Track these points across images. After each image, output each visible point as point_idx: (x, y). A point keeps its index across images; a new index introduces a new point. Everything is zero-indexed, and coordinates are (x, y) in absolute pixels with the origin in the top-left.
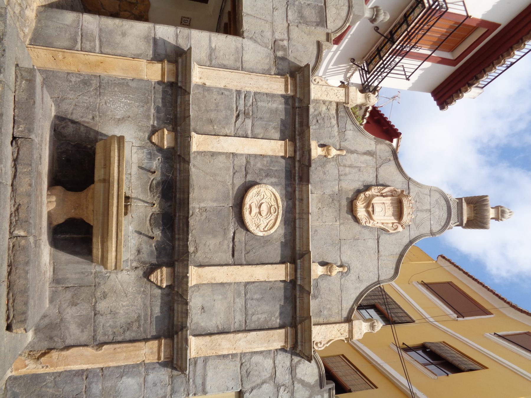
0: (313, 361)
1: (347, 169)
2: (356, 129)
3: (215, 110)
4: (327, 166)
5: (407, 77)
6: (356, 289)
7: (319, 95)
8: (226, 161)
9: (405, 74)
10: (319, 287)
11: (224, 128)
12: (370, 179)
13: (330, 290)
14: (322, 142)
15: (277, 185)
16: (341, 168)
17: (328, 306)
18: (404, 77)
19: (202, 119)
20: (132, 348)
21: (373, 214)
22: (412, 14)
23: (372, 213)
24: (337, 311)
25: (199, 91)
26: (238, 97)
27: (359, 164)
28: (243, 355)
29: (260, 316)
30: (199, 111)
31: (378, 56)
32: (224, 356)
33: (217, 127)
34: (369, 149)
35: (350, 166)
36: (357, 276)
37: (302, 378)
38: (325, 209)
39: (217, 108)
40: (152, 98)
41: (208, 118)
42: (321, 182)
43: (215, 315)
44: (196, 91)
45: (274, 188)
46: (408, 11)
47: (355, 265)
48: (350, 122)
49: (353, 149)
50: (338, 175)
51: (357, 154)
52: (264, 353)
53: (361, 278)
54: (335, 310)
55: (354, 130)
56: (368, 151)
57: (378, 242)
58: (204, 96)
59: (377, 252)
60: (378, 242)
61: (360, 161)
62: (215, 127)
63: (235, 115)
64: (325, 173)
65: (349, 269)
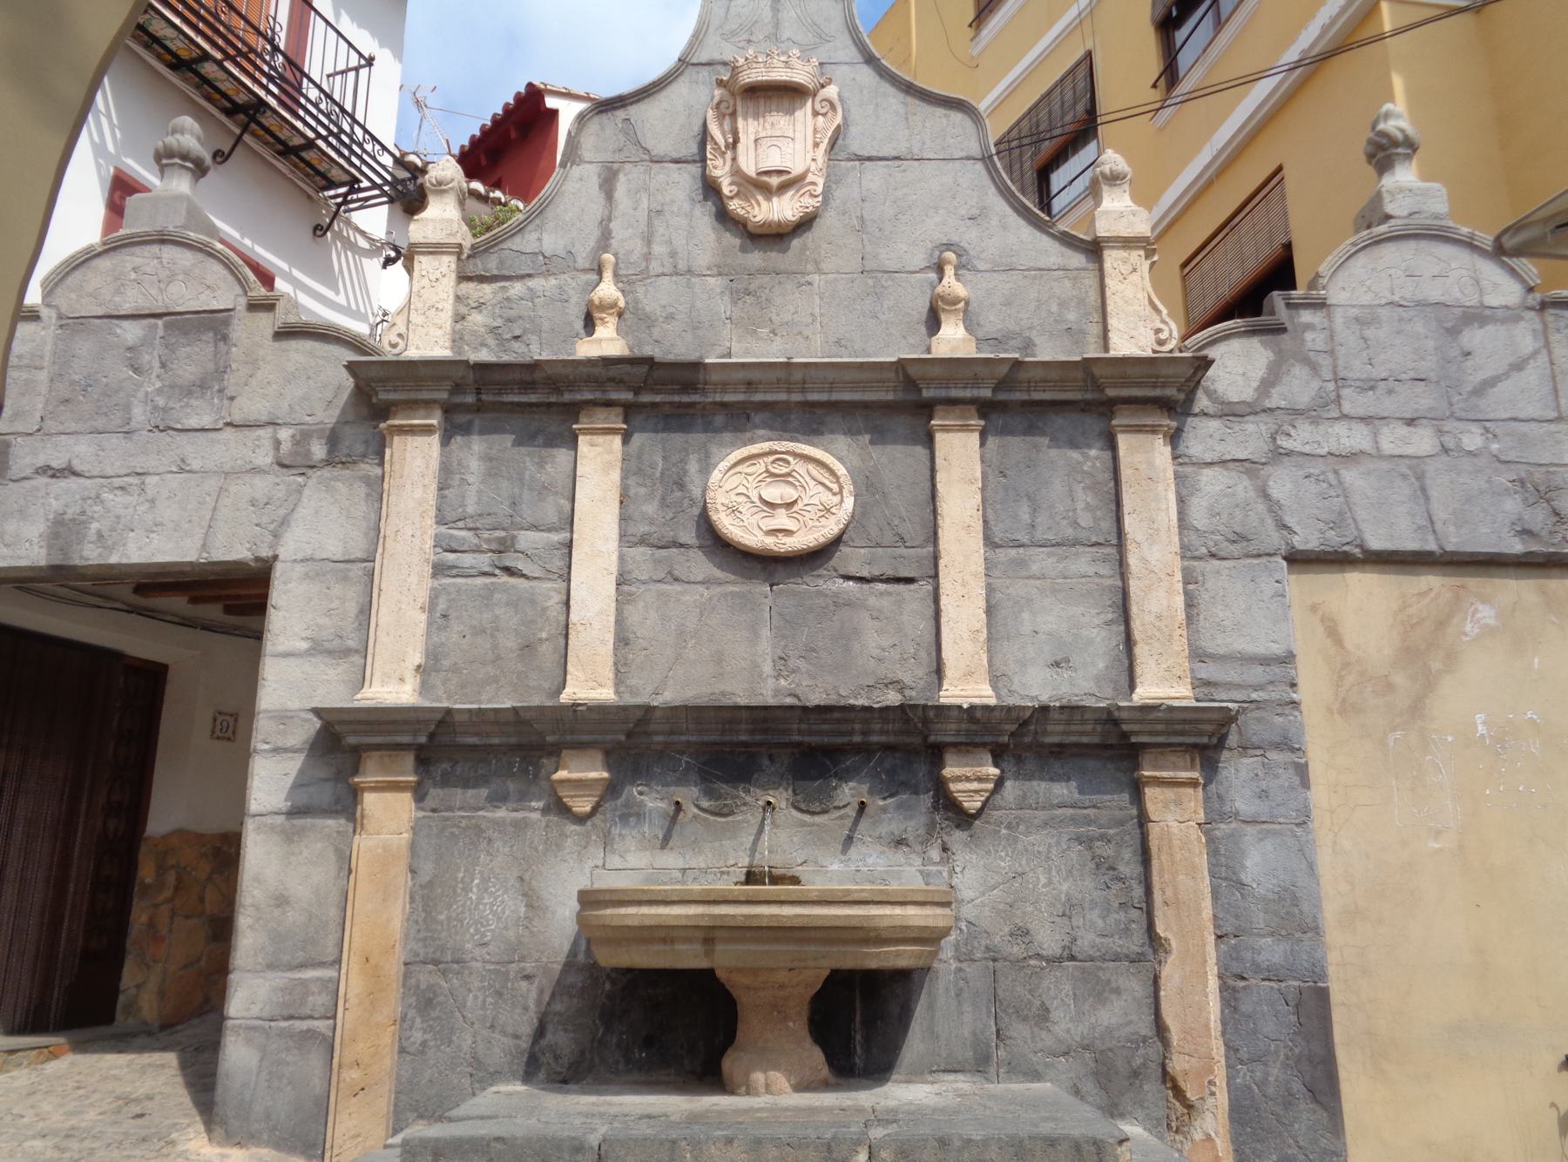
0: (1211, 353)
1: (658, 249)
2: (537, 221)
3: (492, 636)
4: (648, 309)
5: (363, 62)
6: (1004, 227)
7: (440, 332)
8: (642, 603)
9: (357, 69)
10: (999, 336)
11: (545, 609)
12: (683, 182)
13: (1008, 303)
14: (579, 325)
15: (708, 455)
16: (655, 267)
17: (1054, 308)
18: (364, 72)
20: (1163, 858)
21: (789, 173)
22: (168, 43)
23: (784, 178)
24: (1067, 283)
26: (454, 572)
27: (642, 215)
28: (1186, 552)
29: (1080, 505)
31: (304, 154)
32: (1190, 604)
33: (541, 630)
34: (594, 182)
35: (648, 240)
36: (970, 223)
37: (1255, 384)
38: (774, 317)
39: (489, 632)
42: (695, 326)
43: (1075, 631)
44: (440, 693)
45: (716, 466)
46: (159, 57)
47: (936, 228)
48: (517, 239)
49: (597, 233)
50: (674, 278)
51: (610, 220)
52: (1184, 492)
53: (975, 212)
54: (1065, 288)
55: (540, 228)
56: (601, 186)
57: (870, 159)
58: (455, 669)
59: (900, 163)
60: (870, 159)
61: (631, 211)
62: (544, 635)
63: (505, 579)
64: (670, 317)
65: (949, 246)
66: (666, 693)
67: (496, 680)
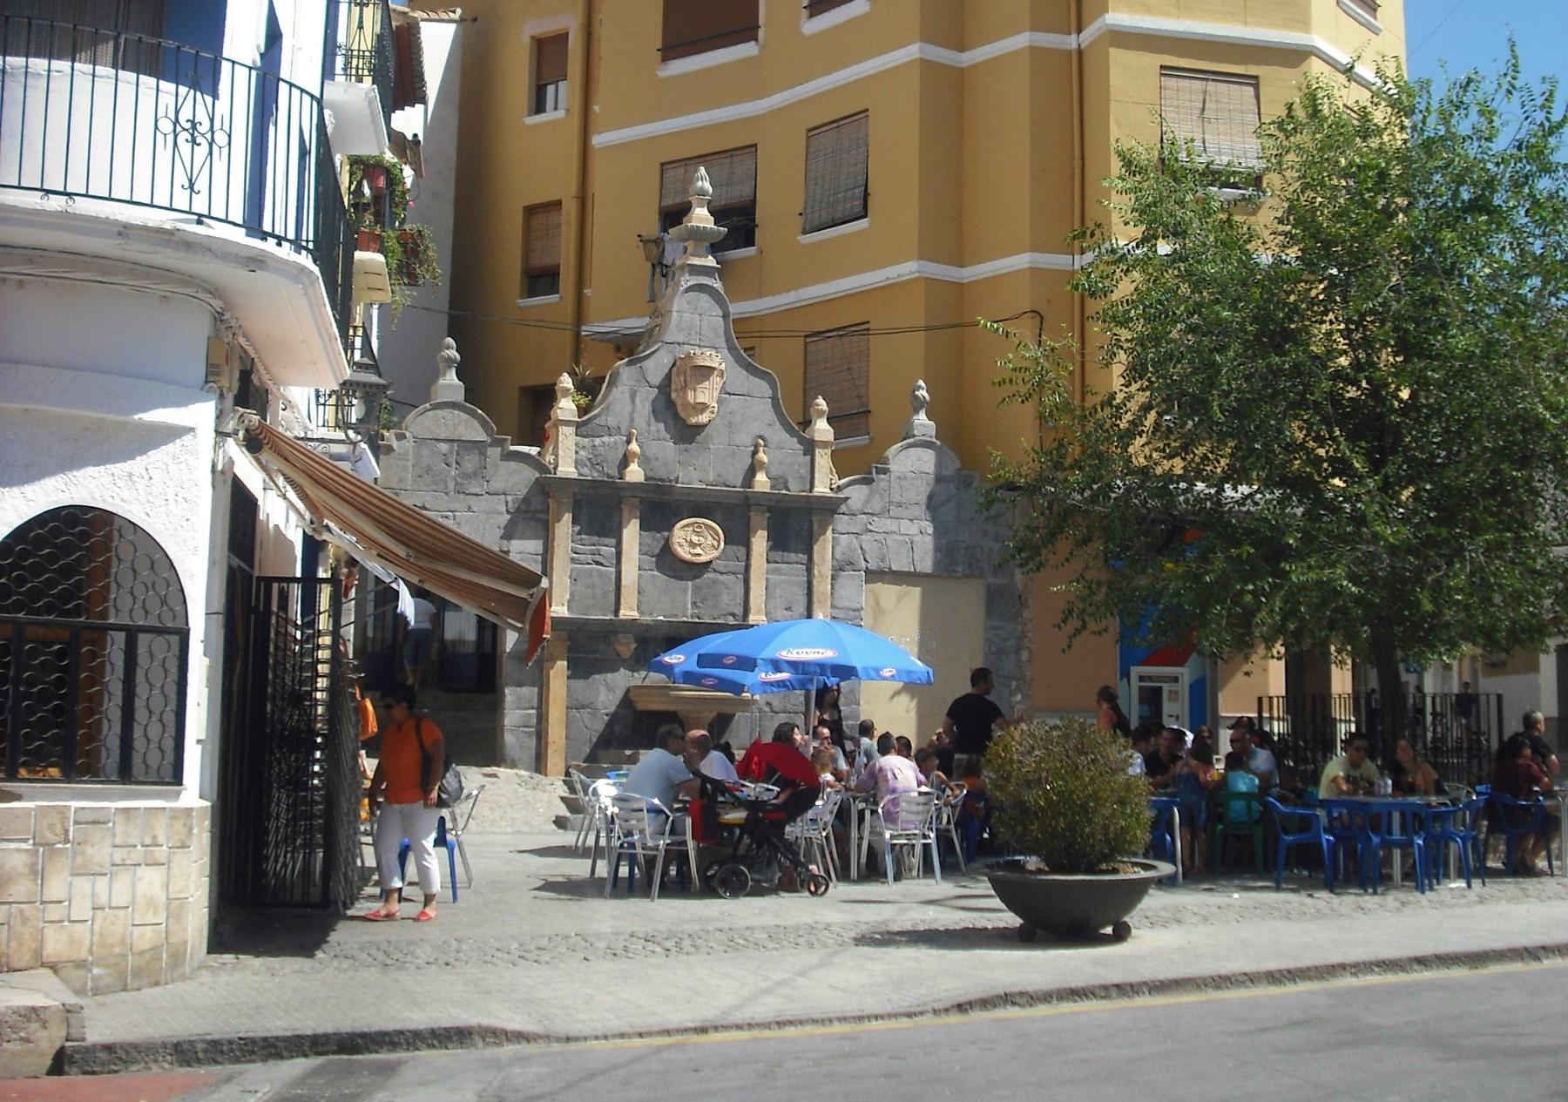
55: (607, 415)
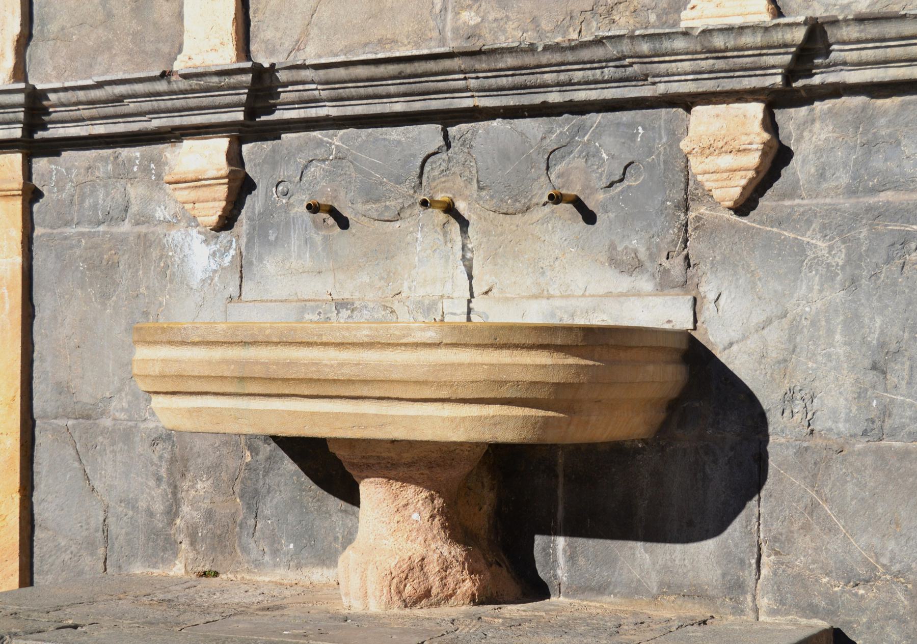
19: (135, 34)
25: (47, 56)
30: (109, 49)
40: (82, 234)
41: (132, 10)
44: (49, 69)
66: (308, 49)
67: (107, 46)
